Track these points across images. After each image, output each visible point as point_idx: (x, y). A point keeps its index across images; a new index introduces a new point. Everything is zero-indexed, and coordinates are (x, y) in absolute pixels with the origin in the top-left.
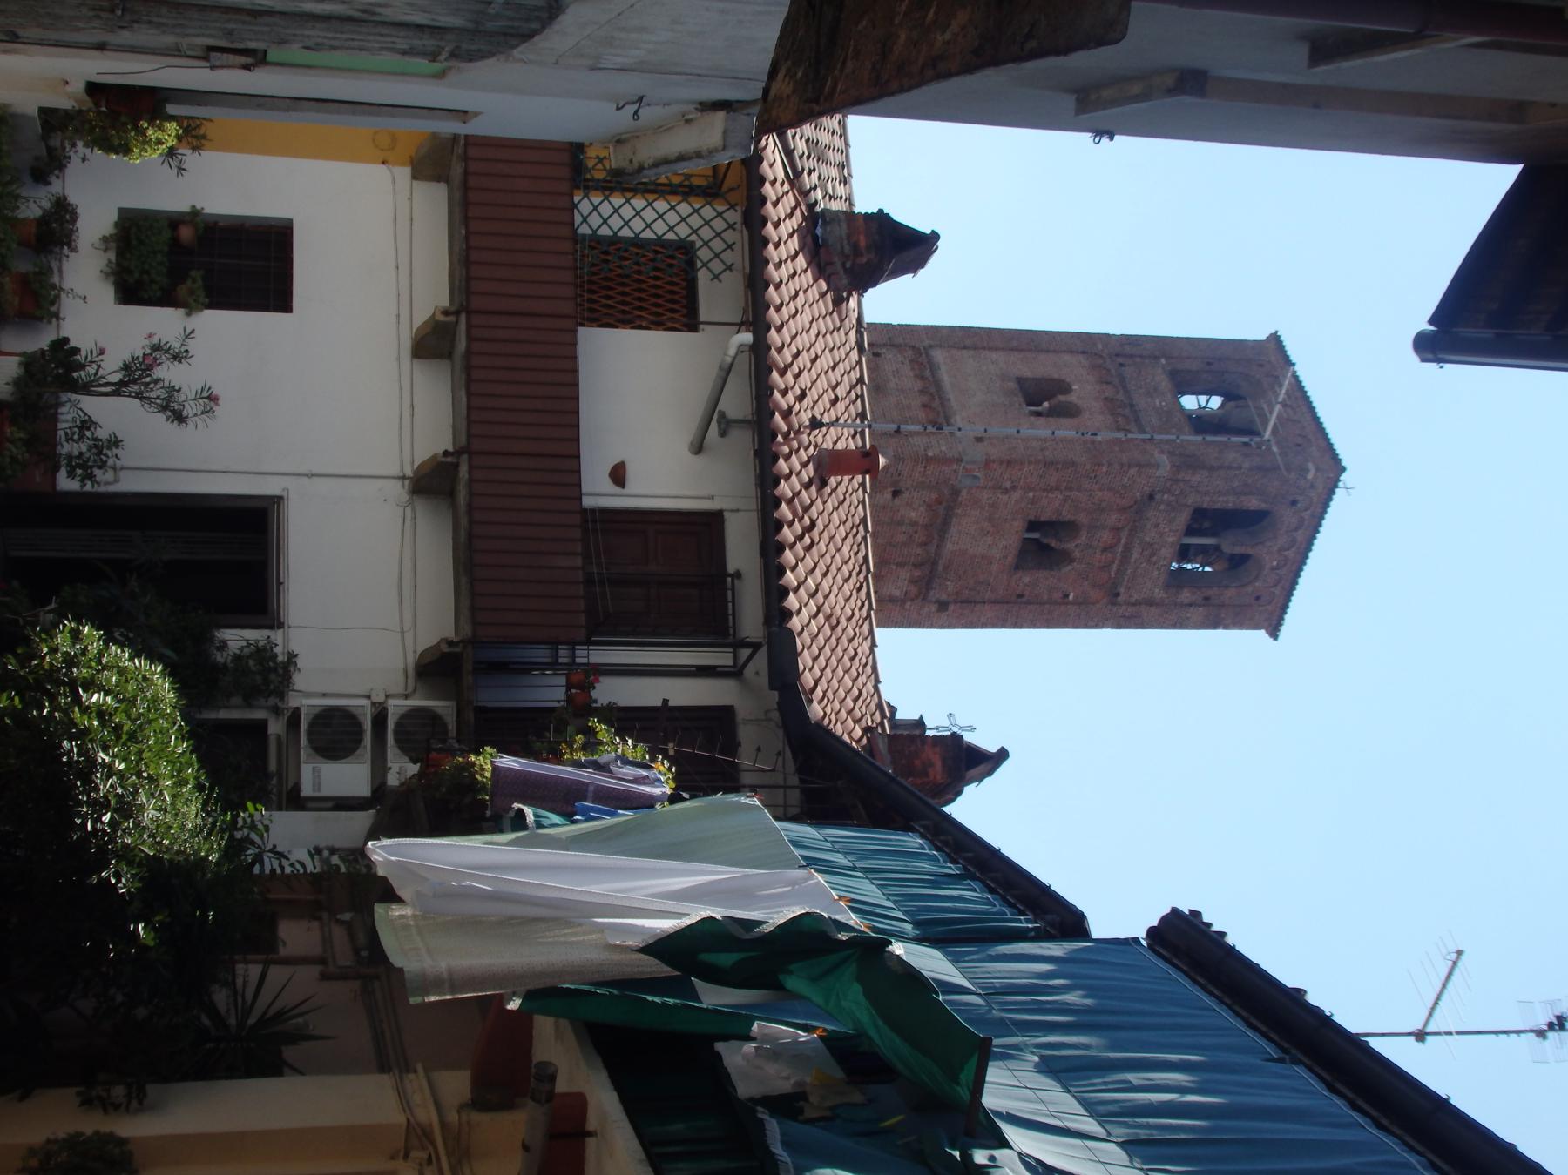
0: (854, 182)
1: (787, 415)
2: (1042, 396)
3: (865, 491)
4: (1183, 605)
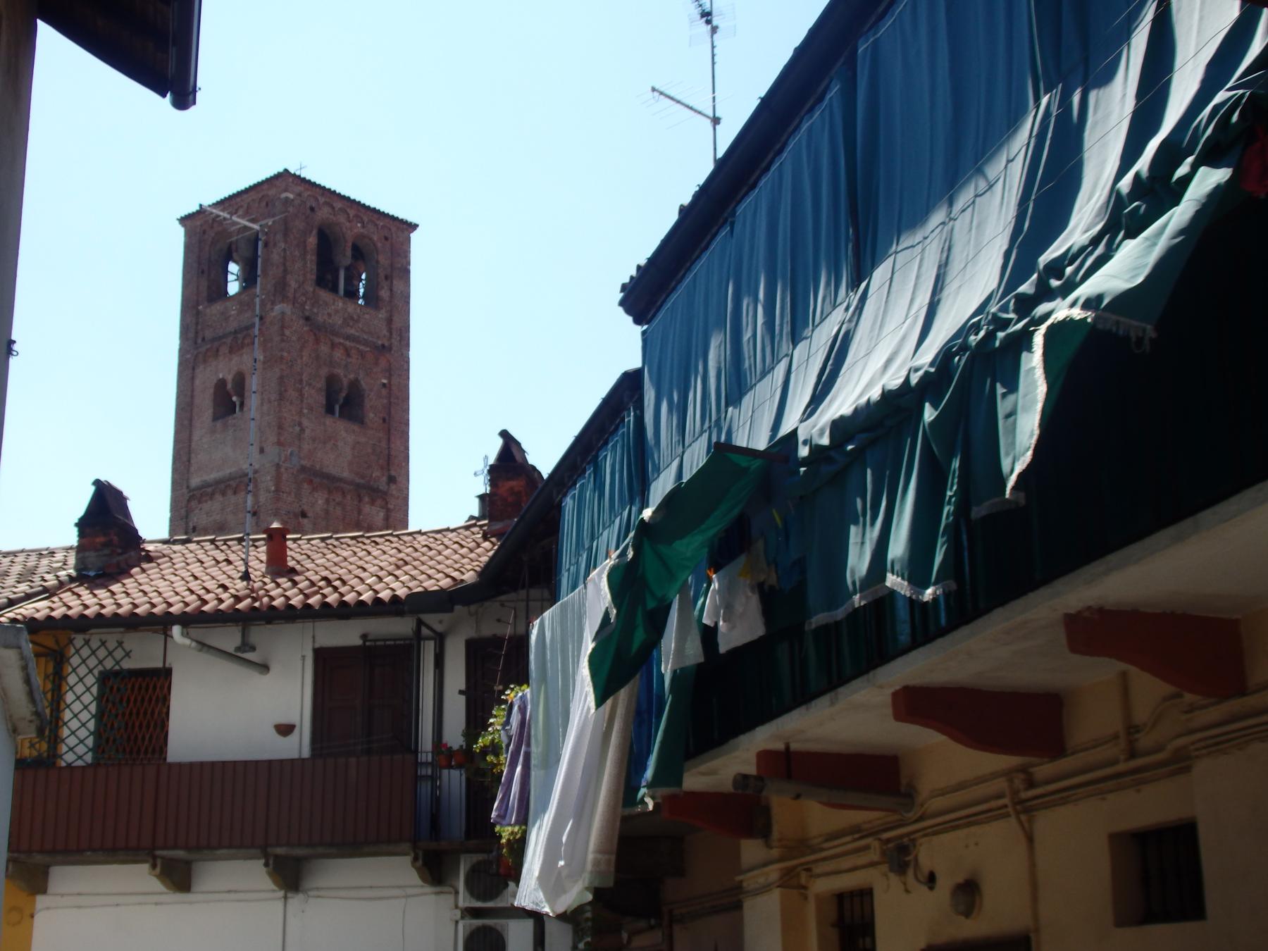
0: (53, 545)
1: (238, 599)
2: (227, 402)
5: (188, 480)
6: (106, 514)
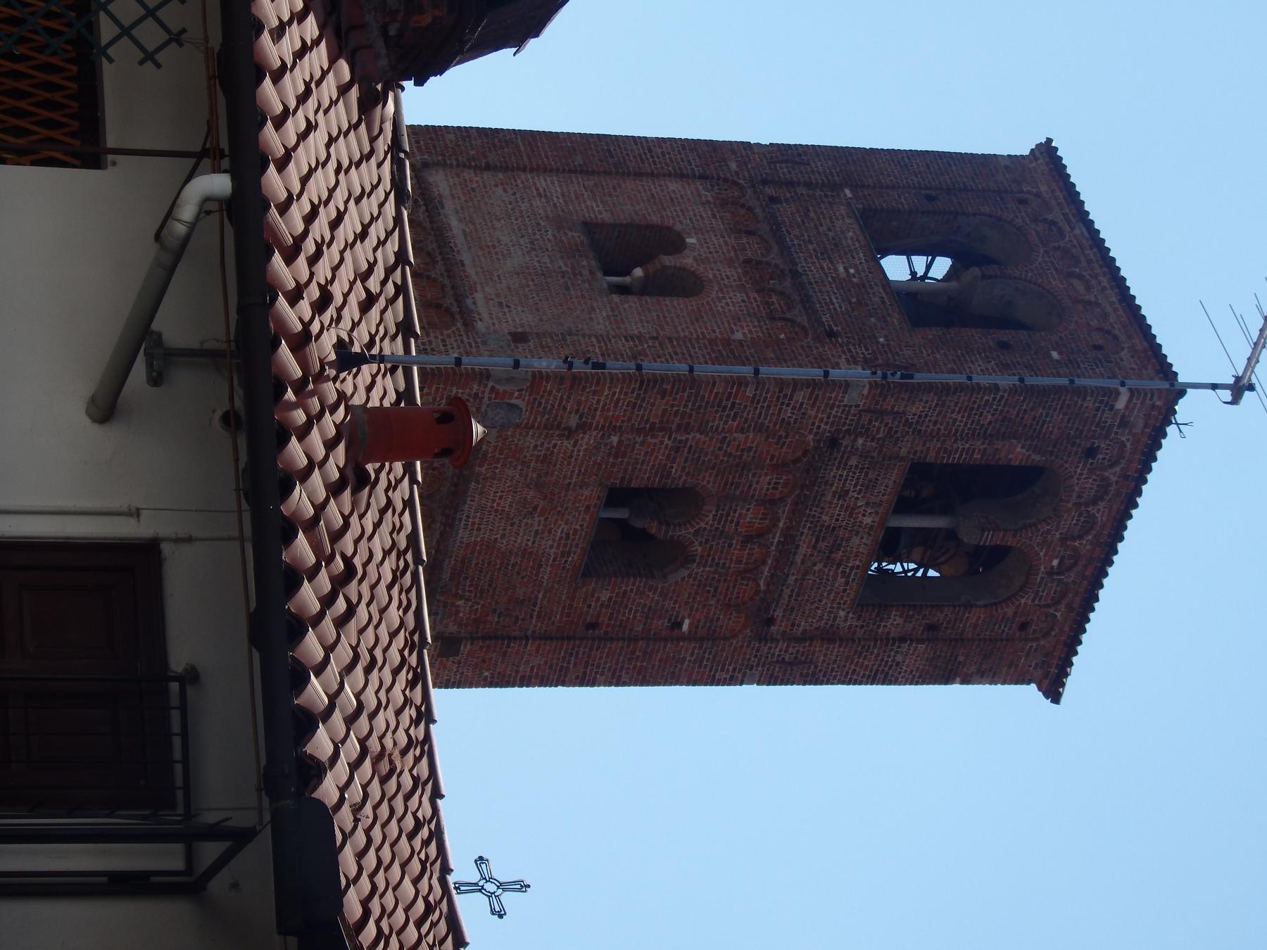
1: (301, 342)
3: (413, 481)
5: (445, 165)
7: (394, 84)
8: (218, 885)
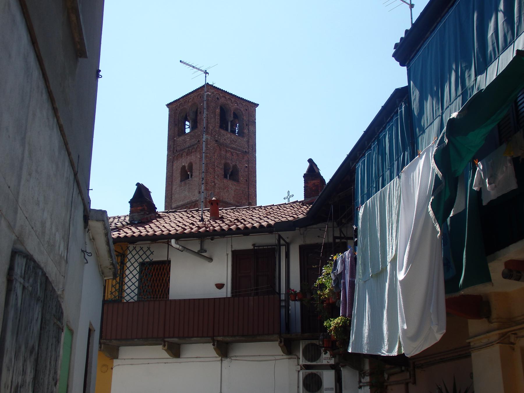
0: (120, 216)
1: (199, 228)
2: (186, 174)
4: (249, 132)
6: (142, 196)
7: (157, 213)
8: (288, 240)
